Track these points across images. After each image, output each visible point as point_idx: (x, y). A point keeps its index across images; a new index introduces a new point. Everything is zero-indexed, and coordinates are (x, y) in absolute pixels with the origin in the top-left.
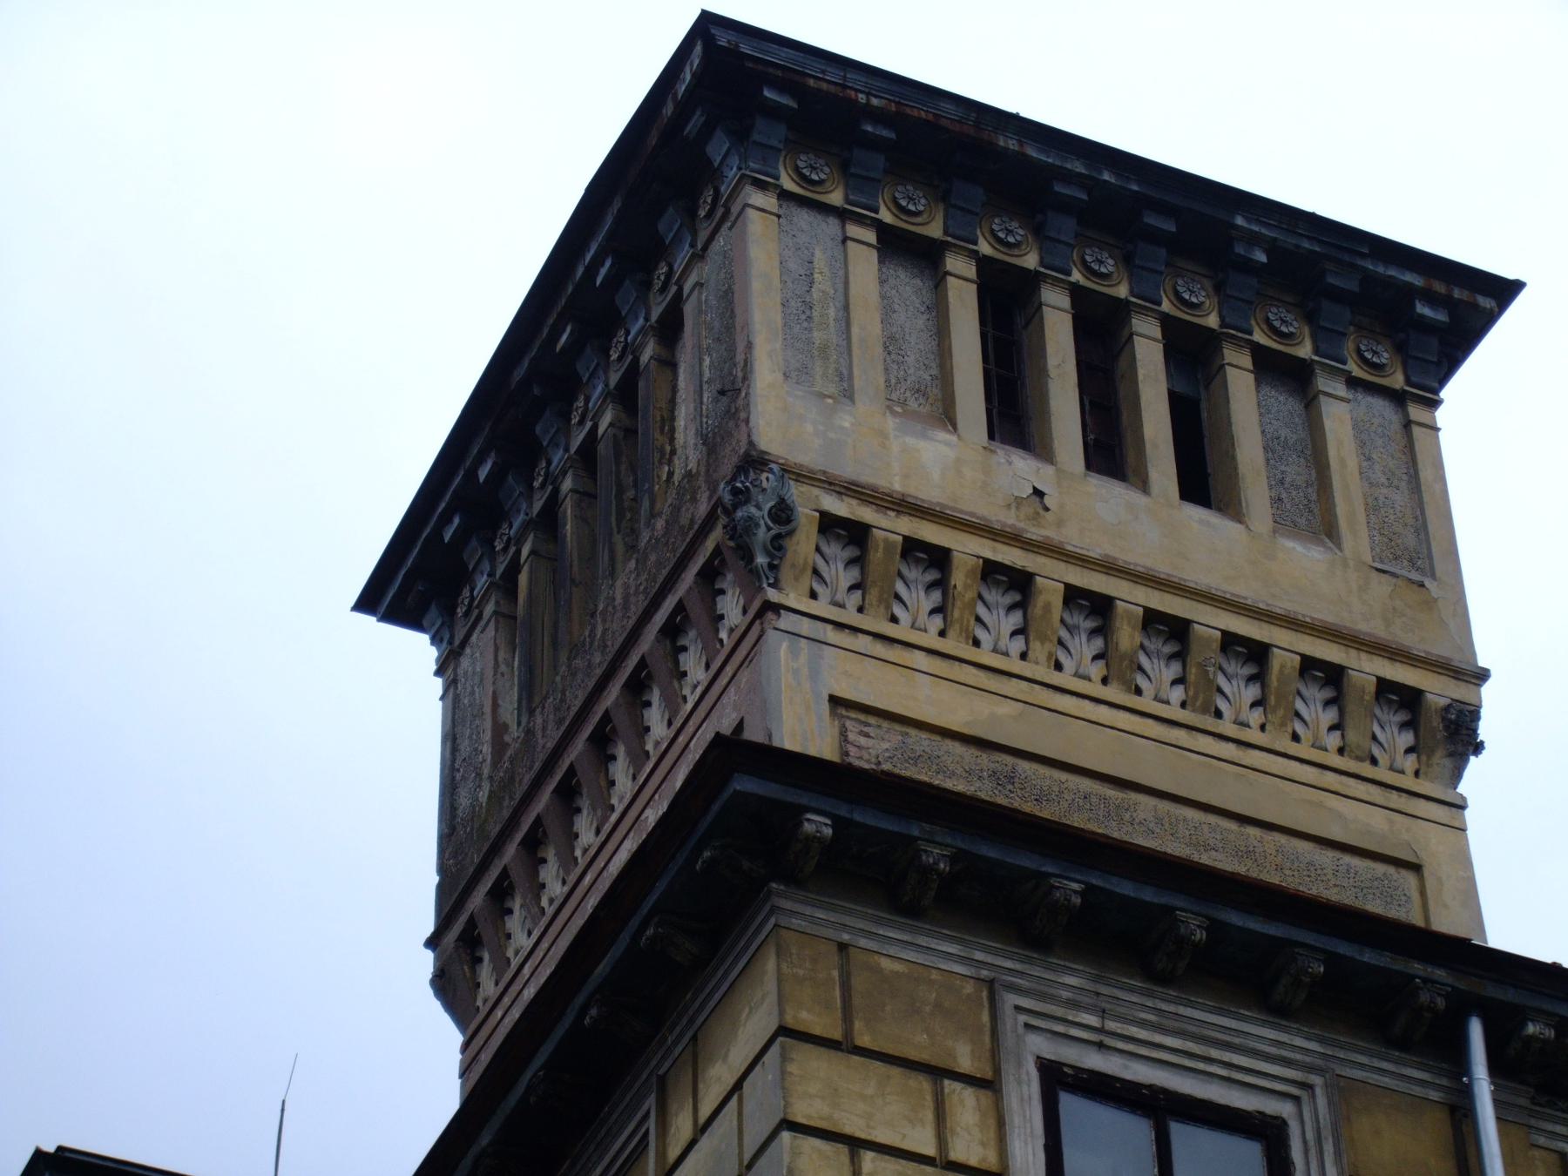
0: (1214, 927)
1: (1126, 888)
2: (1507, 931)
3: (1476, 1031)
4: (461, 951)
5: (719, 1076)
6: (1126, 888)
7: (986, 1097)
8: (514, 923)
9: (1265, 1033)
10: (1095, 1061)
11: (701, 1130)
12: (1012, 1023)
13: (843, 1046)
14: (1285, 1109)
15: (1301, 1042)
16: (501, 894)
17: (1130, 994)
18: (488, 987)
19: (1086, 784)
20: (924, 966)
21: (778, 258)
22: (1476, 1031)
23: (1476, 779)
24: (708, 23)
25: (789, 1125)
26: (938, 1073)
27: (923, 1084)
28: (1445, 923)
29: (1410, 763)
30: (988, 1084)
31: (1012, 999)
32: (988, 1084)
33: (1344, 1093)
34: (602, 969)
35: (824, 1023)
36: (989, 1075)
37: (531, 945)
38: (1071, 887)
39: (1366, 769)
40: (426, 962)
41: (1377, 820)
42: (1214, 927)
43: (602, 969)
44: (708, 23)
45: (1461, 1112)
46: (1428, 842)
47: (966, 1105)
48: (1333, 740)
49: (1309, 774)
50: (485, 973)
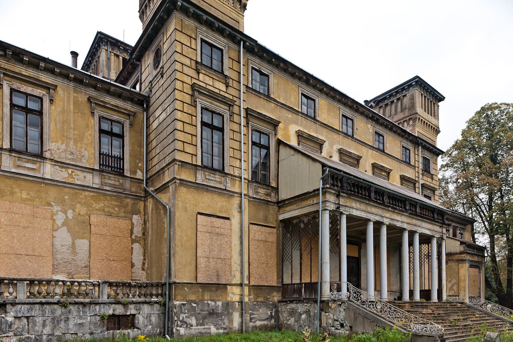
0: (218, 25)
1: (210, 19)
2: (246, 32)
3: (242, 42)
4: (142, 13)
5: (169, 33)
6: (210, 19)
7: (221, 133)
8: (147, 11)
9: (222, 39)
10: (206, 39)
11: (167, 39)
12: (198, 33)
13: (181, 32)
14: (223, 48)
15: (226, 41)
16: (146, 6)
17: (210, 31)
18: (145, 19)
19: (207, 5)
20: (190, 23)
21: (417, 93)
22: (242, 42)
23: (246, 13)
24: (98, 33)
25: (175, 40)
26: (191, 37)
27: (189, 38)
28: (241, 30)
29: (239, 9)
30: (196, 39)
31: (198, 30)
32: (196, 39)
33: (229, 47)
34: (157, 18)
35: (180, 29)
36: (221, 126)
37: (150, 13)
38: (205, 17)
39: (235, 9)
40: (138, 14)
41: (236, 16)
42: (218, 25)
43: (157, 18)
44: (98, 33)
45: (239, 52)
46: (240, 20)
47: (193, 41)
48: (232, 5)
49: (229, 9)
50: (145, 16)
